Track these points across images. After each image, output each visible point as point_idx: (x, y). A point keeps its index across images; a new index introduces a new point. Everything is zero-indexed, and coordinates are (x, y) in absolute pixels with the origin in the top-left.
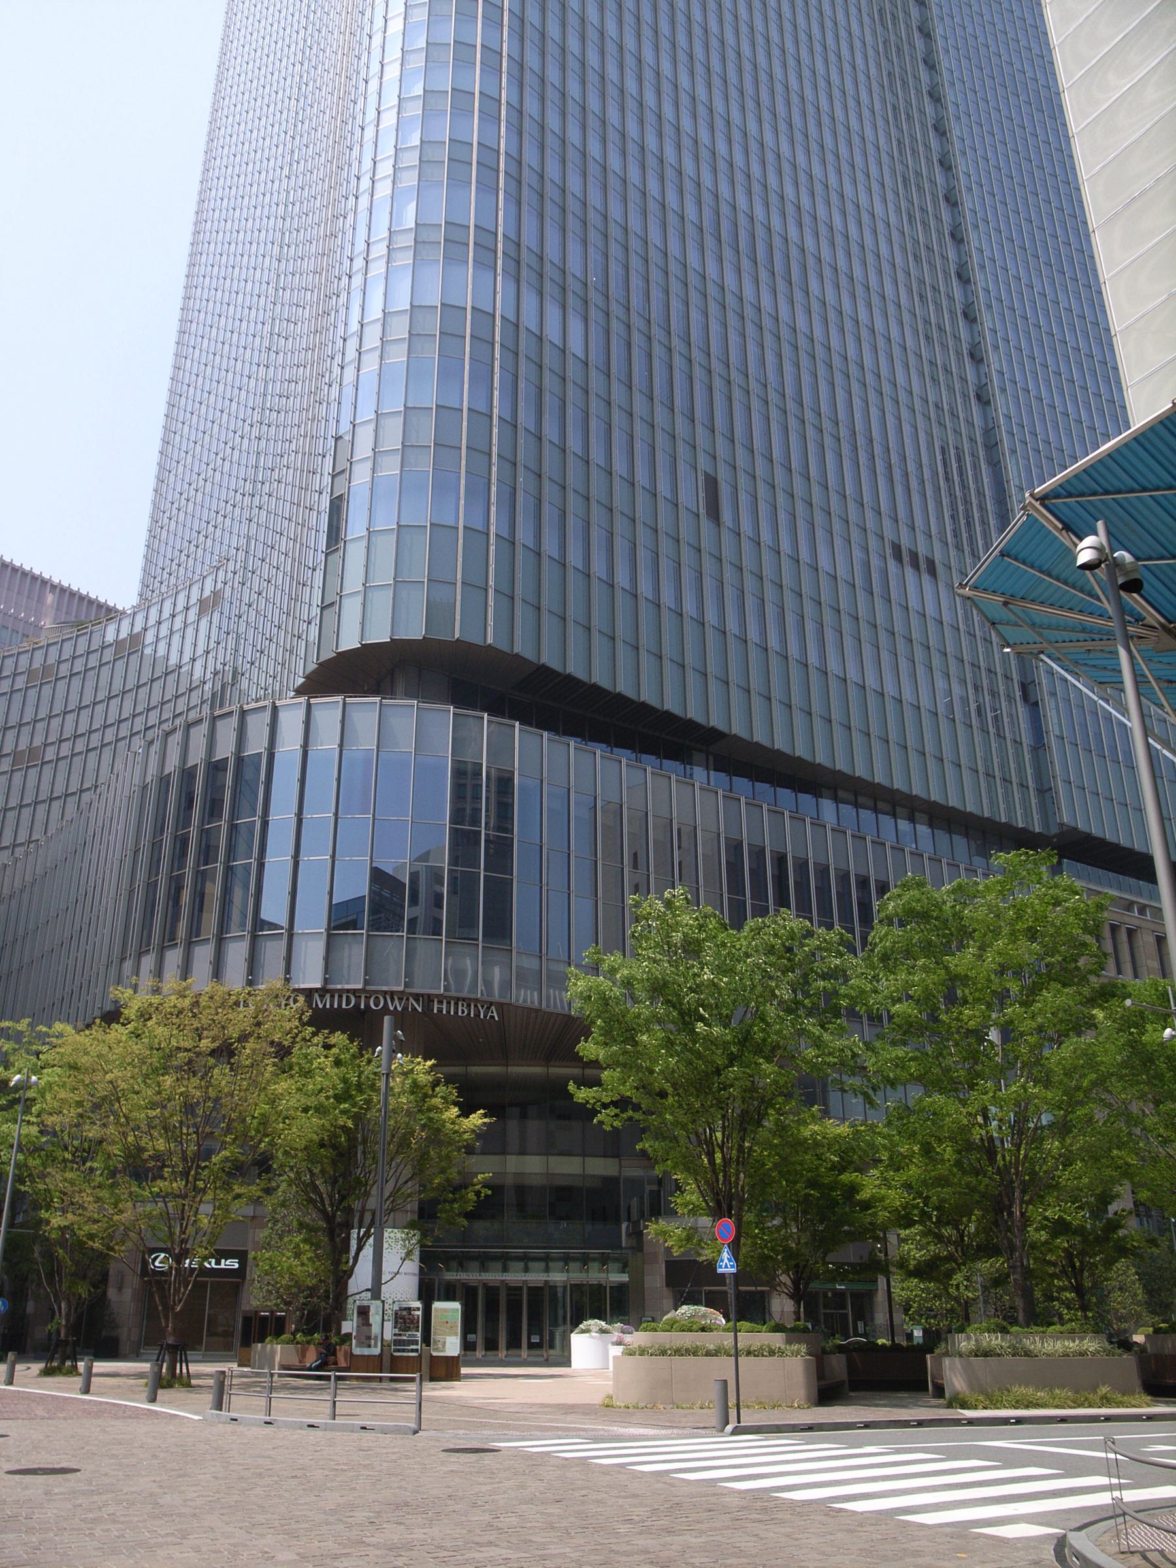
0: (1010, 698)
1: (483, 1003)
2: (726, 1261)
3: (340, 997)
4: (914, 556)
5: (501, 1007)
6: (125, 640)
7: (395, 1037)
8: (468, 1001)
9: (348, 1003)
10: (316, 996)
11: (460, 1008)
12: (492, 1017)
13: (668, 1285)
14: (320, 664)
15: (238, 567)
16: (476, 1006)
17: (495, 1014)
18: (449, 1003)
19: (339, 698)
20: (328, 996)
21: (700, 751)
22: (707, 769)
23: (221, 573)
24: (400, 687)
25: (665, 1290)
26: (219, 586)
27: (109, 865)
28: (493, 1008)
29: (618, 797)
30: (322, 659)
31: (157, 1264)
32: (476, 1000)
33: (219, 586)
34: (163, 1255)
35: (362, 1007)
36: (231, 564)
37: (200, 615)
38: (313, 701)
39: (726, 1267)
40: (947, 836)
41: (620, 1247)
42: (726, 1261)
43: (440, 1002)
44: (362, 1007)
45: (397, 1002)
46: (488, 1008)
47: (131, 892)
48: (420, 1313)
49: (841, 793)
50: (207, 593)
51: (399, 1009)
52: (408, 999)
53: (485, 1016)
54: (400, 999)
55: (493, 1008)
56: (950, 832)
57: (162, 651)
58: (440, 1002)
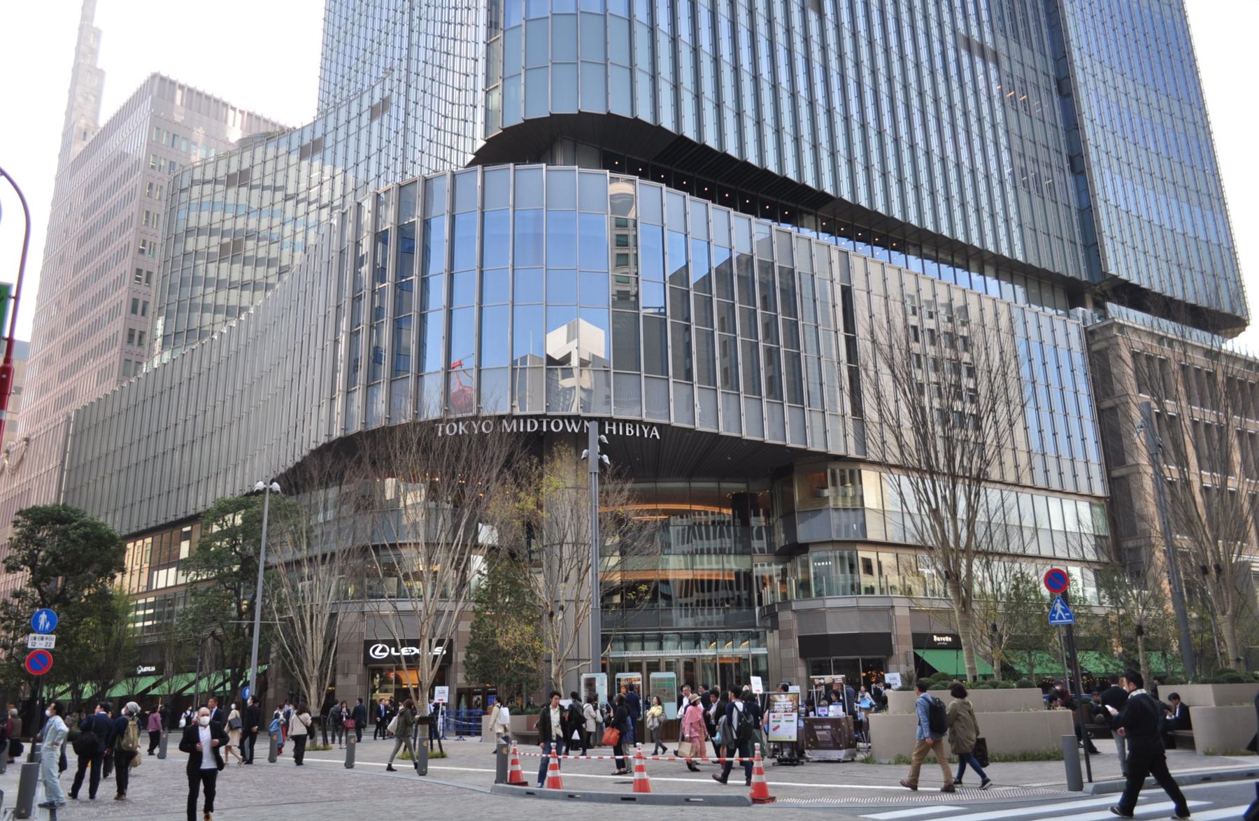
0: (1062, 170)
1: (646, 424)
2: (1060, 611)
3: (525, 423)
4: (982, 47)
5: (661, 427)
6: (308, 145)
7: (600, 442)
8: (633, 423)
9: (532, 427)
10: (504, 422)
11: (627, 429)
12: (654, 436)
13: (801, 656)
14: (504, 130)
15: (325, 178)
16: (640, 427)
17: (657, 434)
18: (618, 426)
19: (511, 165)
20: (515, 422)
21: (809, 214)
22: (817, 230)
23: (388, 82)
24: (559, 159)
25: (800, 661)
26: (387, 93)
27: (306, 330)
28: (655, 428)
29: (749, 250)
30: (506, 126)
31: (377, 652)
32: (641, 422)
33: (387, 93)
34: (380, 646)
35: (545, 430)
36: (396, 73)
37: (372, 119)
38: (486, 169)
39: (1060, 618)
40: (1011, 286)
41: (755, 627)
42: (1060, 611)
43: (611, 425)
44: (545, 430)
45: (573, 425)
46: (651, 429)
47: (336, 341)
48: (640, 683)
49: (925, 251)
50: (377, 100)
51: (576, 431)
52: (583, 423)
53: (649, 435)
54: (577, 423)
55: (655, 428)
56: (1012, 283)
57: (328, 169)
58: (611, 425)
